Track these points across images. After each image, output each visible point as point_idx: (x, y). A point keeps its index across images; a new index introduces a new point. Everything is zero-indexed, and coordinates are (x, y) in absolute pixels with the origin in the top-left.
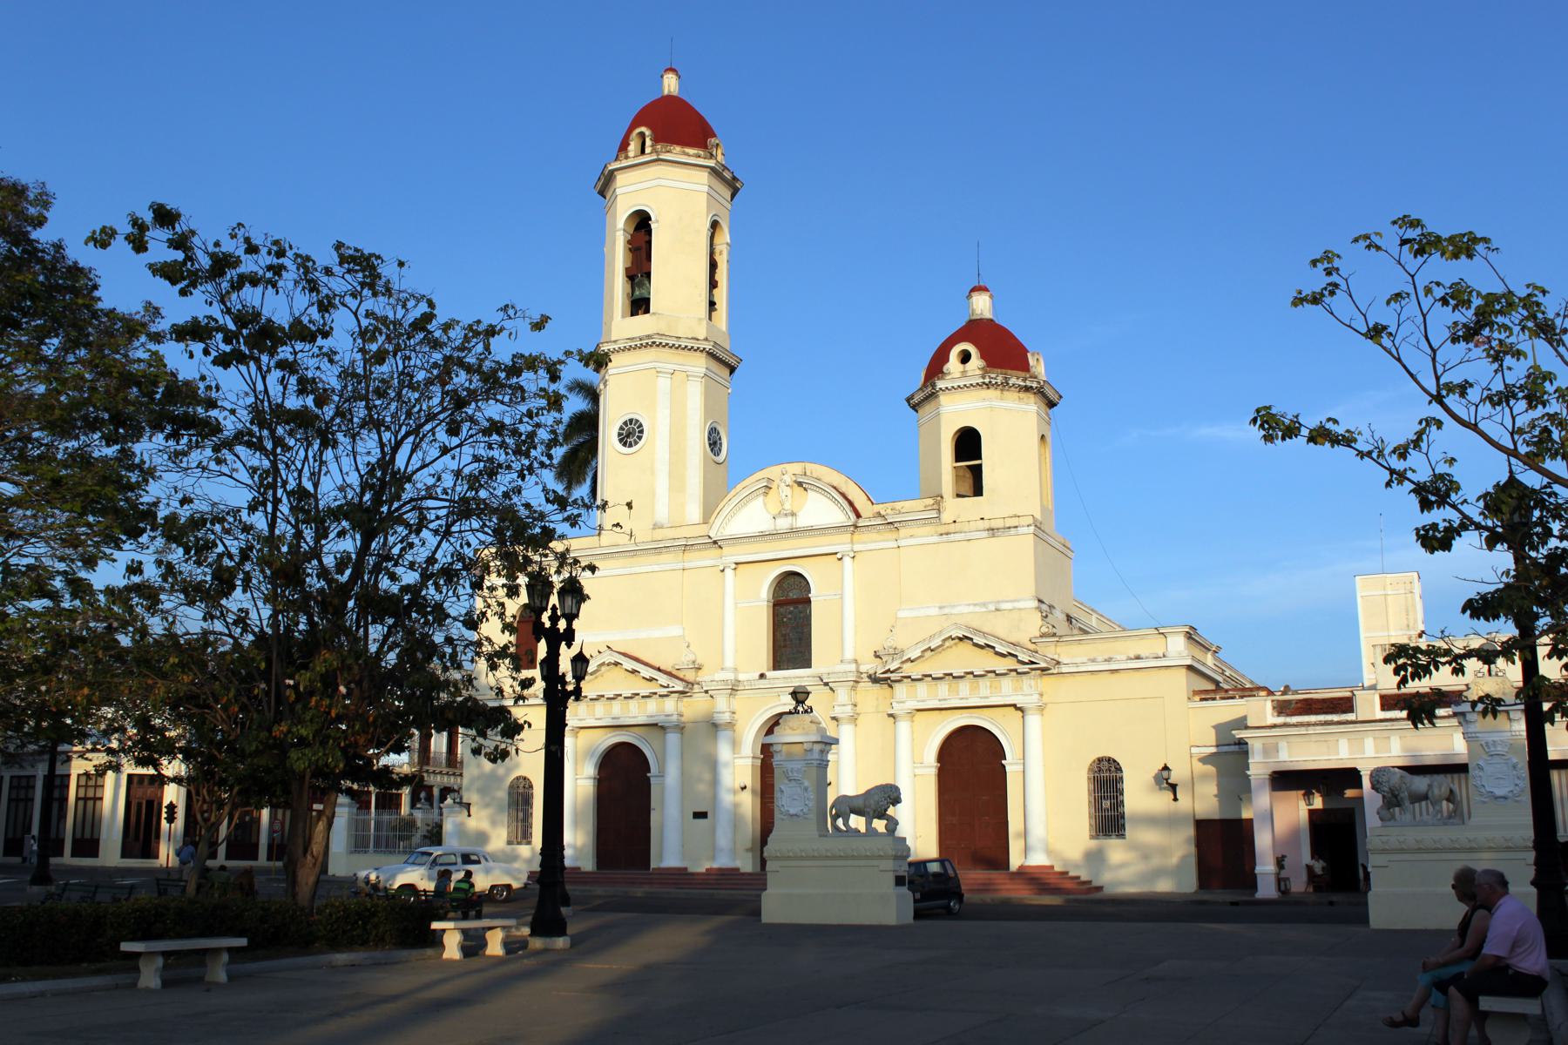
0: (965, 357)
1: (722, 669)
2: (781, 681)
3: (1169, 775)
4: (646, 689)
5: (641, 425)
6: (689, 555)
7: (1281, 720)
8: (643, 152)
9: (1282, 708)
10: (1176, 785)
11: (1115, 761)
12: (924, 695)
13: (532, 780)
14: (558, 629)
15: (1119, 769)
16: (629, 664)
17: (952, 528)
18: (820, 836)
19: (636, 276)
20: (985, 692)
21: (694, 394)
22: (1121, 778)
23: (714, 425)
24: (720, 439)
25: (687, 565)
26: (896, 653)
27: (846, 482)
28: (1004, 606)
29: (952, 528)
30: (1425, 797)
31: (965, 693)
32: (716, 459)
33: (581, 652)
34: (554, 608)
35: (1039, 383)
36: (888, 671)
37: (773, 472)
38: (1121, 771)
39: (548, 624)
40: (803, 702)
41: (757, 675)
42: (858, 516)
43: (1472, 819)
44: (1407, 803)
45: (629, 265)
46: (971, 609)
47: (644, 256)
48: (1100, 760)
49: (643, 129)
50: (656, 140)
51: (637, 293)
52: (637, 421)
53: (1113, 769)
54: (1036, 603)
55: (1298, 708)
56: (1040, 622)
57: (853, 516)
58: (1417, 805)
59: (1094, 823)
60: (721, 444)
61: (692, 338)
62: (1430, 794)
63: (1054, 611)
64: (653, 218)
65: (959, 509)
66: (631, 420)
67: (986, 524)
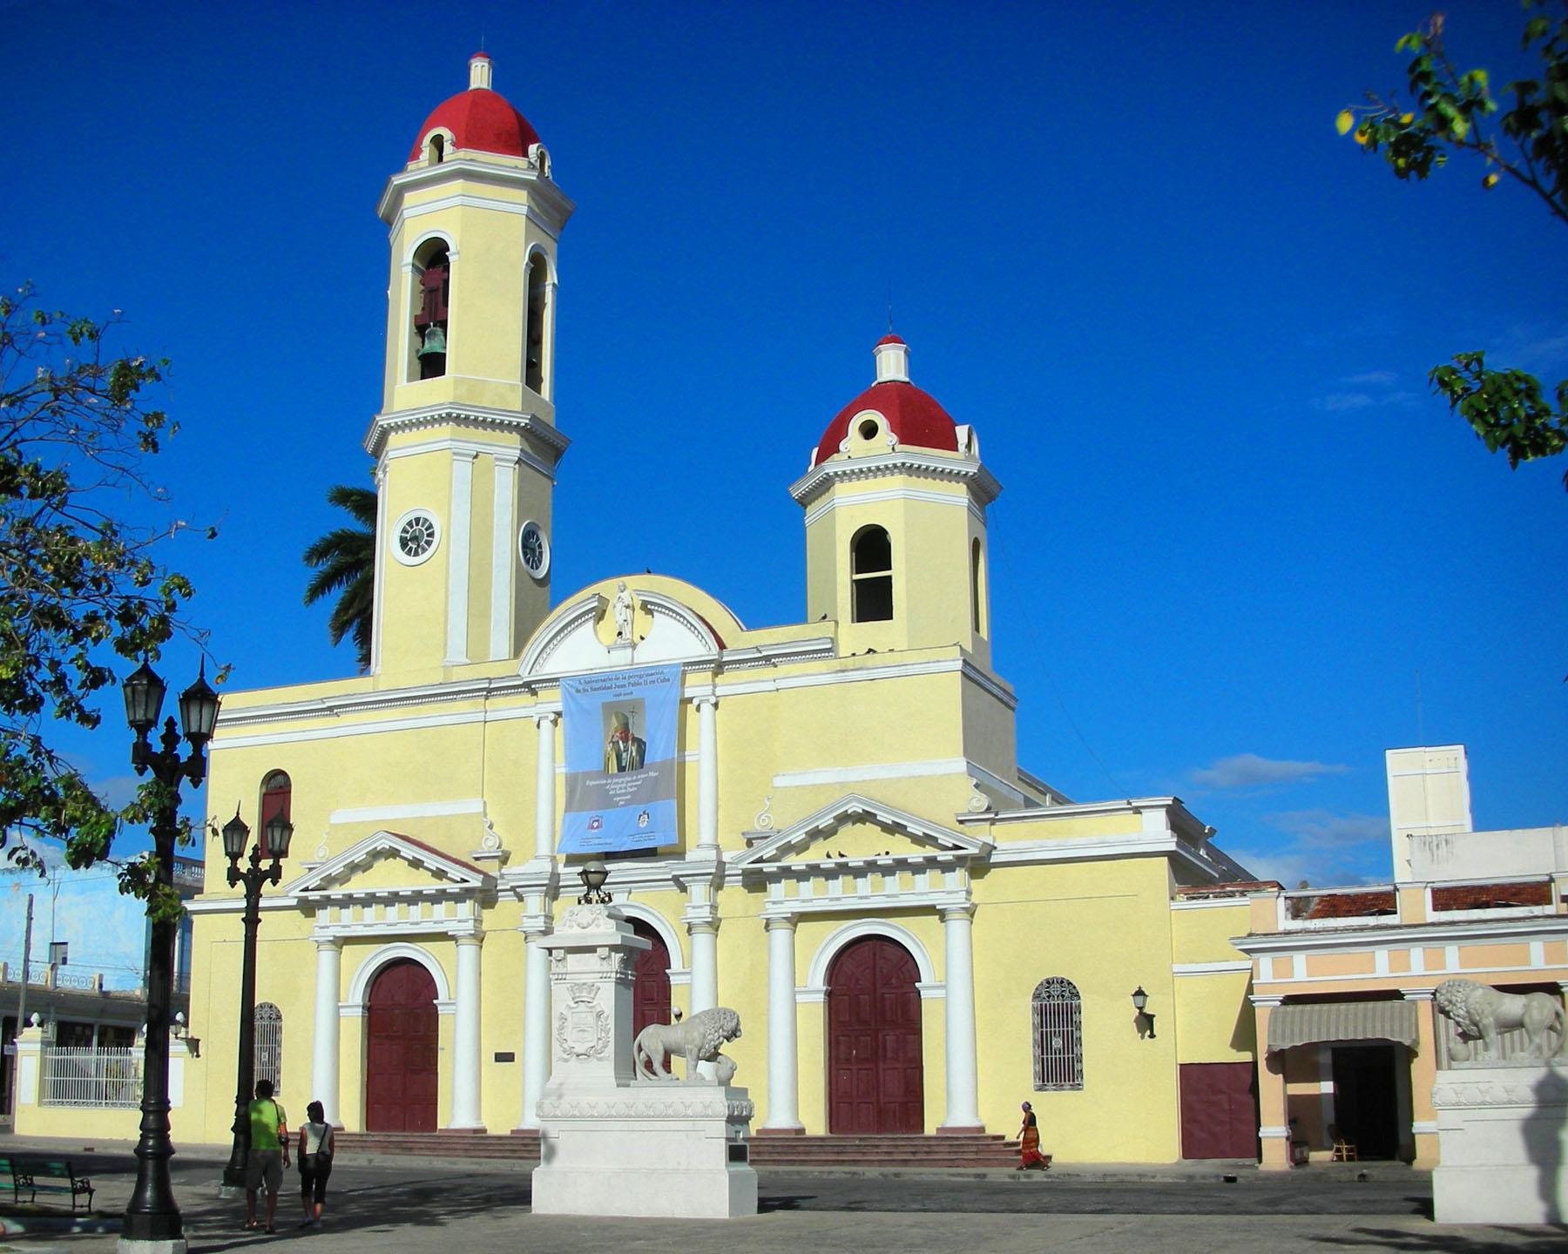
0: (869, 431)
1: (536, 858)
3: (1144, 1002)
4: (430, 885)
5: (430, 526)
6: (497, 702)
8: (440, 159)
9: (1298, 909)
10: (1154, 1016)
11: (1070, 983)
12: (813, 894)
14: (177, 757)
15: (1076, 995)
16: (409, 851)
18: (618, 1086)
20: (897, 891)
21: (505, 483)
22: (1079, 1007)
24: (540, 546)
25: (490, 716)
29: (850, 662)
30: (1519, 1024)
31: (868, 892)
34: (171, 723)
36: (760, 860)
37: (608, 587)
38: (1079, 998)
39: (158, 747)
40: (598, 888)
42: (722, 646)
45: (419, 312)
47: (441, 299)
51: (427, 345)
53: (1067, 994)
55: (1318, 911)
57: (715, 648)
58: (1507, 1035)
59: (1159, 1179)
60: (541, 553)
62: (1527, 1020)
65: (855, 636)
66: (417, 520)
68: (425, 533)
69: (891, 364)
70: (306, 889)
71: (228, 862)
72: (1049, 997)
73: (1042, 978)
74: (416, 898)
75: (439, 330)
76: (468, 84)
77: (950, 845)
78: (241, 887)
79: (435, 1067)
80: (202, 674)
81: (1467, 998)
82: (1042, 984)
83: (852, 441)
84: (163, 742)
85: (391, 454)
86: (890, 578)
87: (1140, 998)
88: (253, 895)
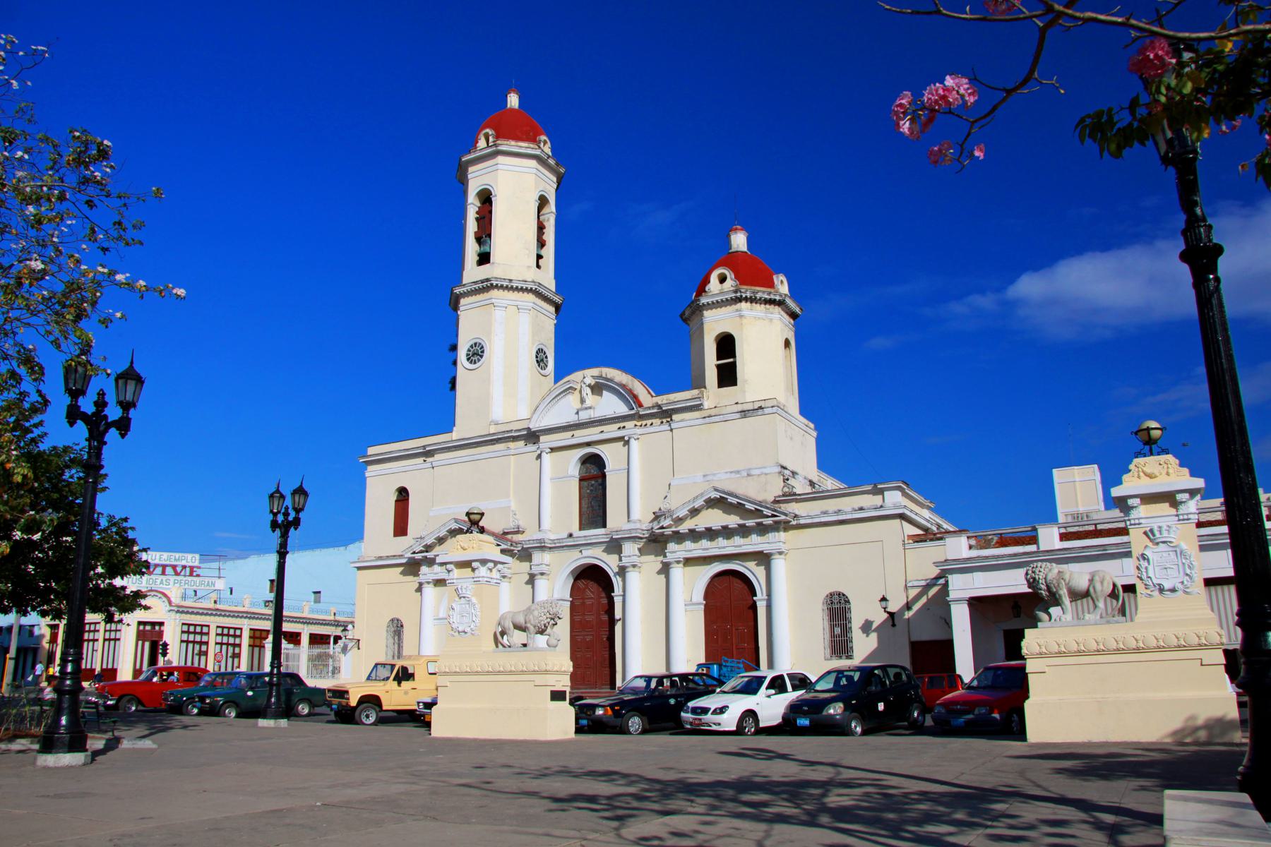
0: (722, 279)
2: (583, 539)
5: (482, 347)
7: (974, 553)
11: (844, 595)
13: (403, 621)
15: (848, 602)
17: (713, 412)
19: (482, 237)
22: (849, 609)
23: (540, 347)
26: (668, 514)
27: (632, 380)
28: (753, 472)
32: (542, 372)
33: (301, 486)
35: (781, 296)
36: (662, 528)
41: (565, 535)
43: (1138, 615)
44: (1066, 600)
46: (728, 475)
48: (832, 595)
49: (487, 130)
50: (497, 137)
51: (482, 249)
52: (480, 344)
53: (843, 601)
54: (779, 469)
56: (782, 484)
58: (1079, 602)
61: (523, 281)
63: (796, 476)
64: (493, 194)
65: (713, 394)
66: (475, 344)
67: (740, 408)
68: (480, 351)
69: (739, 241)
70: (414, 553)
71: (271, 517)
72: (832, 603)
73: (828, 592)
74: (727, 532)
75: (488, 239)
76: (507, 106)
77: (770, 515)
78: (278, 532)
79: (318, 637)
80: (132, 363)
81: (1046, 575)
82: (827, 596)
83: (714, 285)
84: (95, 406)
85: (461, 308)
86: (718, 359)
87: (884, 603)
88: (285, 536)
